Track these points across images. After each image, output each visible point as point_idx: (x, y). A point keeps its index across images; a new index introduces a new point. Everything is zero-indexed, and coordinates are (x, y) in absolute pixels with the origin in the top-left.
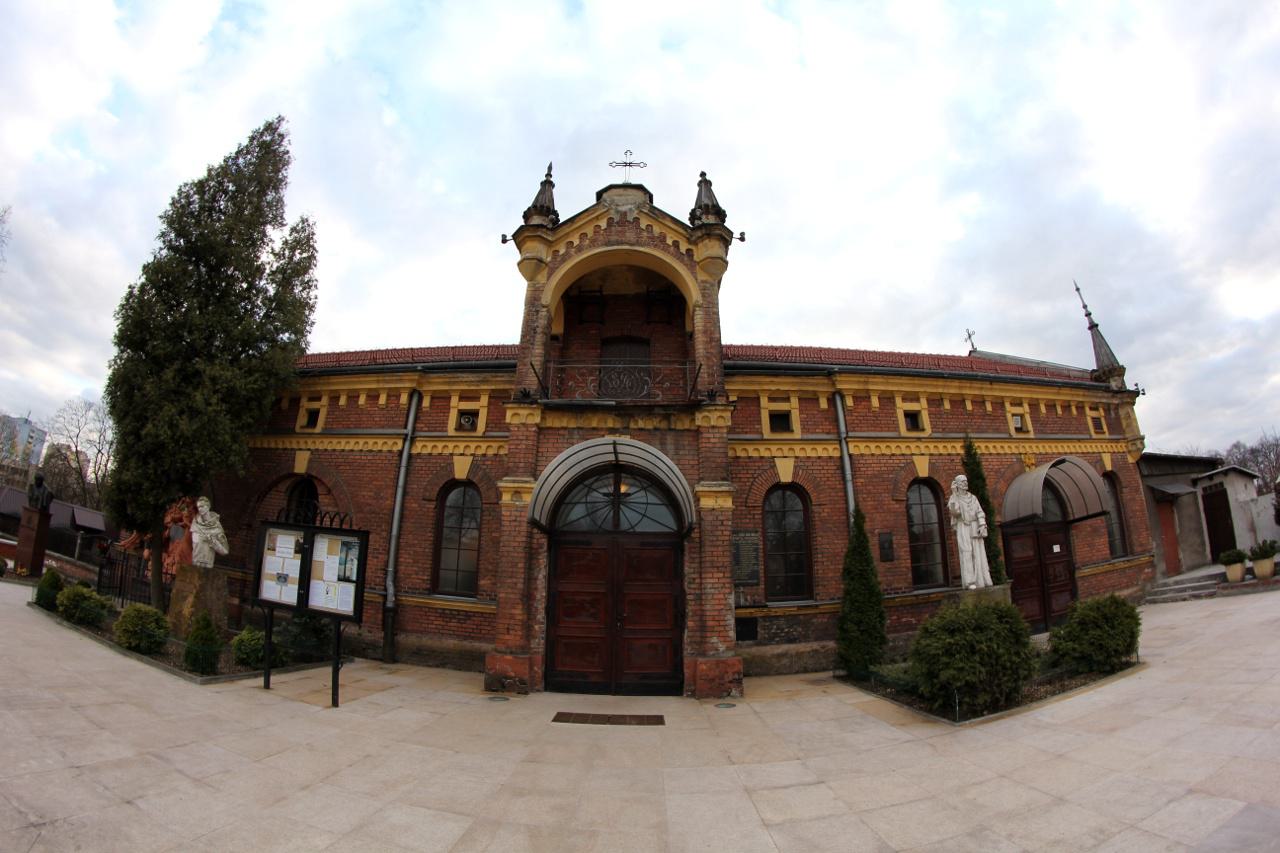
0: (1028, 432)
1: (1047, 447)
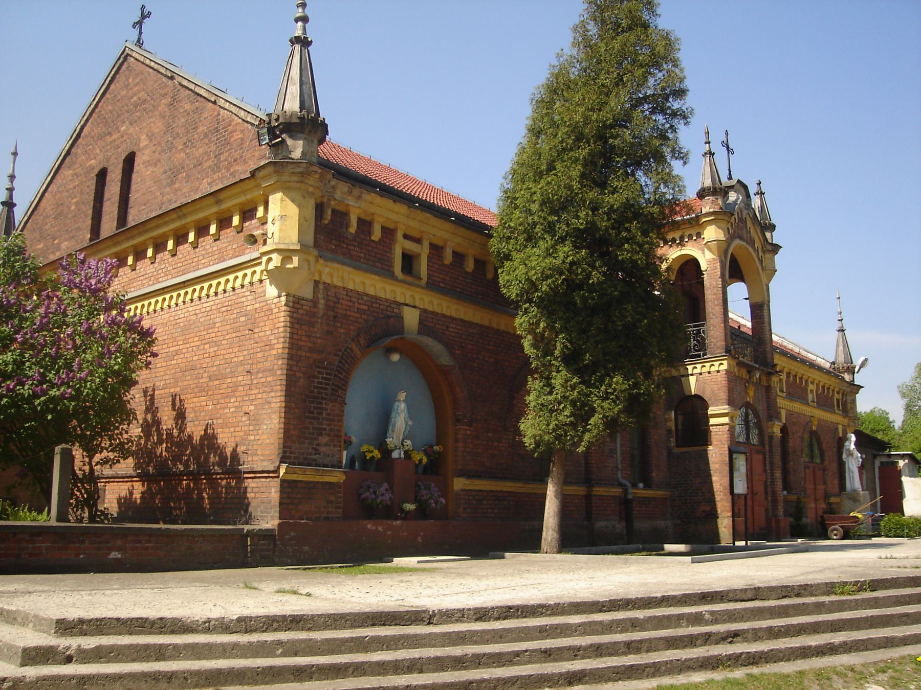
0: (420, 279)
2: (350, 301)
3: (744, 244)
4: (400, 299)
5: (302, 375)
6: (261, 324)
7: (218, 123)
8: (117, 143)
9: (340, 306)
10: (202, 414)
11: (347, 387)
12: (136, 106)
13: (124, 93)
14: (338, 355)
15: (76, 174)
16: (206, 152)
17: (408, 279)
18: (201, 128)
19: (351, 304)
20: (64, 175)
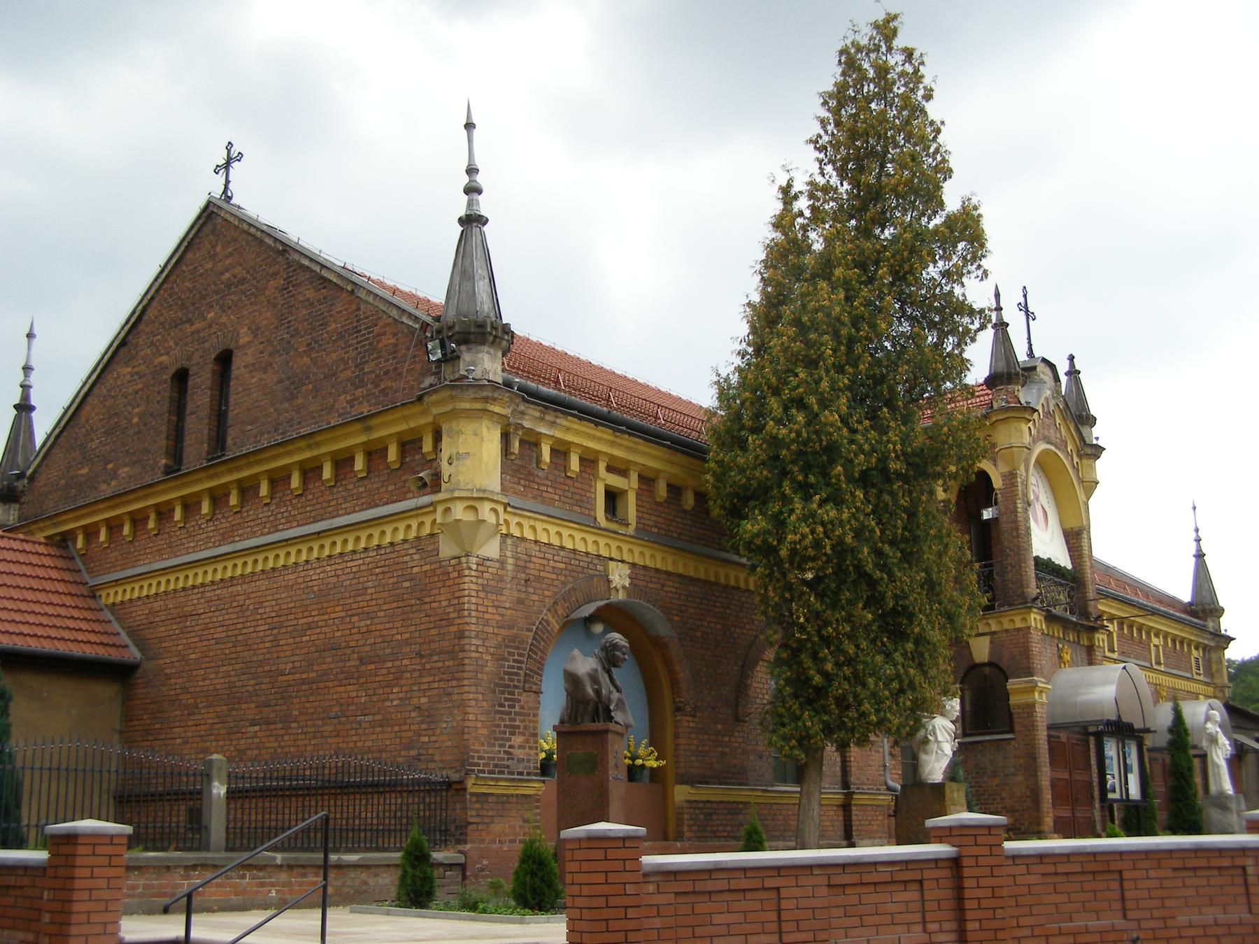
0: (627, 525)
1: (670, 562)
2: (544, 558)
3: (1053, 448)
4: (604, 552)
5: (489, 657)
6: (433, 592)
7: (358, 321)
8: (202, 335)
9: (532, 566)
10: (351, 708)
11: (541, 669)
12: (229, 286)
13: (209, 266)
14: (530, 630)
15: (138, 373)
16: (342, 359)
17: (614, 526)
18: (333, 326)
19: (545, 562)
20: (118, 373)
